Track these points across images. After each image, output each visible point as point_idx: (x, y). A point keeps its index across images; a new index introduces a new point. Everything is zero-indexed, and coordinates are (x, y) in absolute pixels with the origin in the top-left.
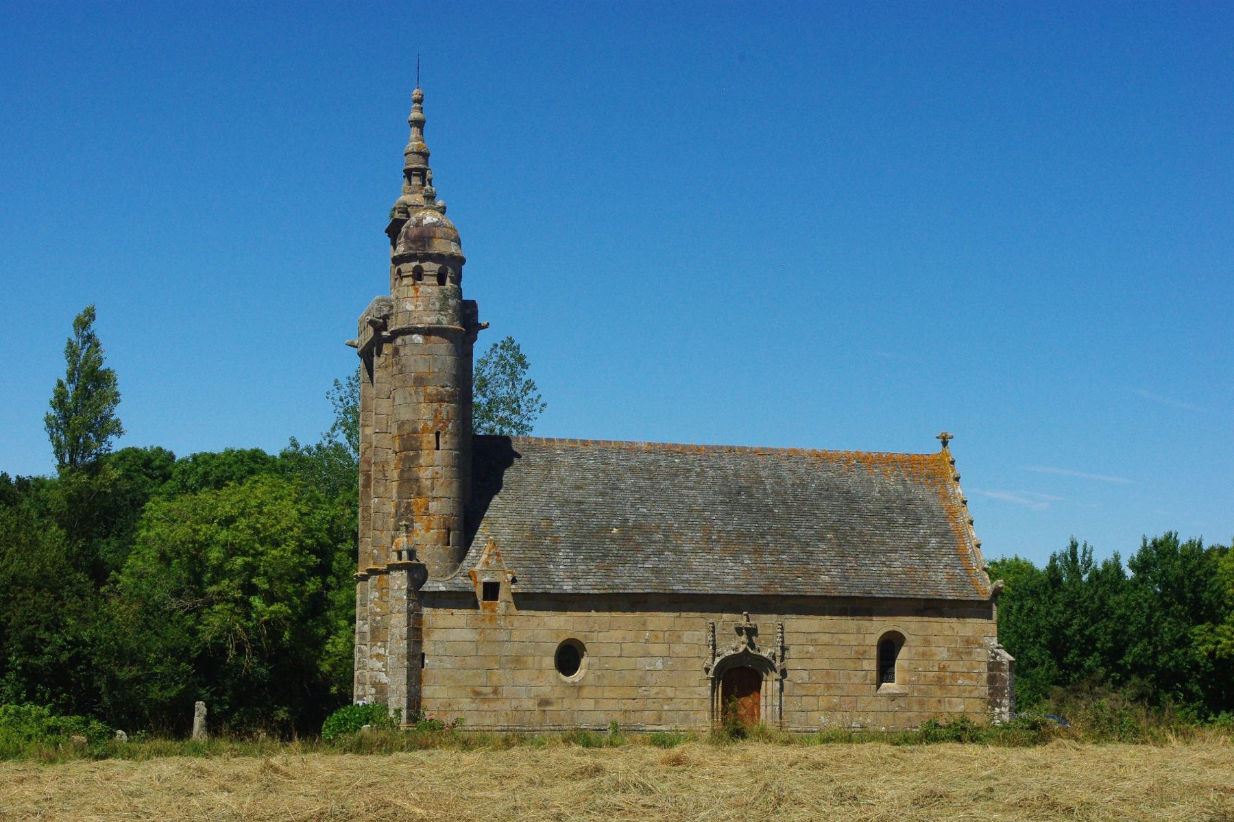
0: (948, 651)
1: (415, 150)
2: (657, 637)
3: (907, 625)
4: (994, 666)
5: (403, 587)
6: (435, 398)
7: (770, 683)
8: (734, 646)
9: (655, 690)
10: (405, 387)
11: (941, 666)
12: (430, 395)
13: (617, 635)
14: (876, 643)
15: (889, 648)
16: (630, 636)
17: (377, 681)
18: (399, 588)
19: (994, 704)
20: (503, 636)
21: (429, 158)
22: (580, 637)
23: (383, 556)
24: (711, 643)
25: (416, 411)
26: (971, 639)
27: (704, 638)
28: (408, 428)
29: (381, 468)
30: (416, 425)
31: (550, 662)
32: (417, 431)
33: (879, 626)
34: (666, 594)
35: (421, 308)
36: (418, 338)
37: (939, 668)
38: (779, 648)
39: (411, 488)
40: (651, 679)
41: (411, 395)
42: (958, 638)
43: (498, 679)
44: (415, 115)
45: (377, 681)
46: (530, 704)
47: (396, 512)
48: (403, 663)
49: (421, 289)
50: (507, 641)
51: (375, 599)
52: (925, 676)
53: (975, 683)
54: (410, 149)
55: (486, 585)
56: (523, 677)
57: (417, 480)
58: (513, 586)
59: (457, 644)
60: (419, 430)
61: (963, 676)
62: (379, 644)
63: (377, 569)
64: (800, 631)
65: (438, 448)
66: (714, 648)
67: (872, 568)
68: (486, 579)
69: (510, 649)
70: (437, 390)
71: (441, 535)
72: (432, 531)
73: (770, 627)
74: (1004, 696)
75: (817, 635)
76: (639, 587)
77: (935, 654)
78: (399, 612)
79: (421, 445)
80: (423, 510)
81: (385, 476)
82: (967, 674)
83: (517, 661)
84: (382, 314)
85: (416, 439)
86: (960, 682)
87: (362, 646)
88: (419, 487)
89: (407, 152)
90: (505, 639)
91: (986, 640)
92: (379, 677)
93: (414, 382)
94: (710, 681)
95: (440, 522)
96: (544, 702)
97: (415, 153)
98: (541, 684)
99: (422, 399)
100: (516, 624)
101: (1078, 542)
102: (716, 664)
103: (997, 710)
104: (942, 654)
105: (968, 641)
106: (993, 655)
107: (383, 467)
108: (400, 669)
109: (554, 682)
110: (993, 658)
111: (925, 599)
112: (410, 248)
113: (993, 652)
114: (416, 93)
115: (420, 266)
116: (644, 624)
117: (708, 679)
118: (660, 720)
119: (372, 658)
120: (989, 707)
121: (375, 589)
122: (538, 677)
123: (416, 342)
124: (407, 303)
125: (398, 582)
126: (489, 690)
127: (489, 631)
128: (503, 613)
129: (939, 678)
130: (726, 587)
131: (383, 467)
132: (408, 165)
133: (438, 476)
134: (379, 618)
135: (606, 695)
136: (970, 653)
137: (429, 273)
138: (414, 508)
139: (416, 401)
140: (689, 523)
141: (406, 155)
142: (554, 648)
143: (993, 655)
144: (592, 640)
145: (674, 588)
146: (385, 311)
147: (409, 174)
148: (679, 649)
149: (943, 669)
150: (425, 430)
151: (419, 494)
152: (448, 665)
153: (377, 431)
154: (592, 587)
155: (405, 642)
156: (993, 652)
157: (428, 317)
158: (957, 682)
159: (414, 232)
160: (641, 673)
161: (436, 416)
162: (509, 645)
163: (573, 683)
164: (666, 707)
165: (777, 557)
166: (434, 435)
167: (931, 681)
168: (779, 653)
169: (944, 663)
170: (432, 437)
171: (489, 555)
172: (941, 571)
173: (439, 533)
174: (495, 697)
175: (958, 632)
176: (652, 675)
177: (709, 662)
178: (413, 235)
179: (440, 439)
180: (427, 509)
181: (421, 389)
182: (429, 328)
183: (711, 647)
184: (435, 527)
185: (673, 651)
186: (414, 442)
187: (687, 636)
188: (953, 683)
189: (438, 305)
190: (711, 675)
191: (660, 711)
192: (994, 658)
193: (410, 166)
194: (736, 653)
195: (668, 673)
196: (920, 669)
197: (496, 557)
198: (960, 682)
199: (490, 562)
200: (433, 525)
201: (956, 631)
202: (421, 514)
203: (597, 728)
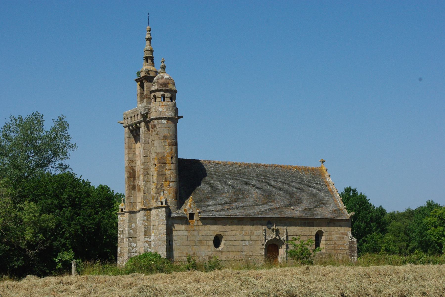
0: (337, 237)
1: (150, 50)
2: (246, 233)
3: (324, 229)
5: (164, 215)
6: (171, 144)
7: (282, 249)
8: (271, 236)
9: (246, 253)
10: (159, 140)
11: (335, 243)
12: (169, 143)
13: (234, 232)
14: (315, 235)
15: (319, 236)
16: (238, 233)
17: (147, 251)
18: (162, 215)
19: (351, 255)
20: (196, 233)
21: (153, 52)
22: (221, 233)
23: (147, 204)
24: (264, 235)
25: (164, 149)
26: (344, 233)
27: (262, 233)
28: (161, 155)
29: (146, 170)
30: (164, 154)
31: (212, 243)
32: (165, 156)
33: (315, 230)
34: (250, 217)
36: (164, 121)
37: (334, 243)
38: (285, 237)
40: (245, 249)
42: (340, 232)
43: (195, 250)
44: (148, 36)
45: (147, 251)
47: (156, 187)
48: (165, 244)
50: (198, 235)
51: (145, 220)
52: (330, 246)
53: (345, 248)
54: (147, 49)
55: (190, 214)
56: (203, 248)
57: (165, 175)
58: (199, 215)
59: (181, 236)
60: (166, 156)
61: (341, 246)
63: (146, 208)
64: (291, 230)
65: (172, 163)
66: (266, 237)
67: (310, 208)
68: (190, 212)
69: (199, 238)
70: (171, 141)
71: (174, 196)
72: (171, 194)
73: (282, 229)
74: (355, 253)
75: (297, 232)
76: (241, 215)
77: (333, 238)
78: (162, 224)
79: (166, 162)
81: (148, 173)
82: (343, 245)
83: (201, 242)
84: (146, 112)
85: (164, 159)
86: (340, 248)
87: (130, 238)
88: (166, 177)
89: (145, 50)
90: (197, 234)
91: (348, 233)
93: (163, 138)
94: (264, 249)
95: (174, 191)
97: (149, 50)
98: (209, 251)
99: (166, 144)
100: (200, 229)
101: (430, 200)
102: (266, 243)
104: (335, 238)
105: (343, 234)
106: (351, 238)
107: (147, 170)
108: (163, 246)
109: (213, 250)
110: (351, 239)
111: (330, 219)
112: (160, 87)
113: (350, 237)
114: (148, 28)
116: (242, 228)
117: (263, 248)
119: (144, 242)
120: (350, 257)
121: (145, 216)
122: (208, 249)
123: (163, 123)
124: (159, 108)
125: (161, 213)
126: (192, 253)
127: (191, 231)
128: (196, 225)
129: (334, 247)
130: (268, 215)
131: (147, 170)
132: (146, 55)
133: (173, 173)
134: (147, 227)
135: (230, 255)
136: (343, 238)
137: (168, 97)
139: (164, 145)
140: (249, 191)
141: (144, 51)
142: (213, 237)
143: (351, 238)
144: (225, 234)
145: (252, 215)
146: (147, 111)
147: (146, 58)
148: (253, 237)
149: (335, 244)
151: (166, 180)
152: (178, 244)
153: (145, 156)
154: (225, 215)
155: (165, 236)
156: (350, 237)
158: (339, 248)
159: (161, 81)
160: (241, 246)
161: (171, 151)
162: (198, 237)
163: (219, 250)
165: (280, 204)
166: (171, 158)
167: (332, 248)
168: (285, 239)
169: (336, 242)
170: (170, 158)
171: (191, 203)
172: (331, 209)
173: (174, 195)
174: (194, 256)
175: (340, 231)
176: (245, 247)
177: (264, 242)
178: (161, 82)
179: (173, 159)
180: (169, 186)
181: (166, 140)
182: (169, 118)
183: (264, 237)
185: (252, 238)
186: (163, 160)
187: (256, 233)
188: (339, 249)
189: (171, 109)
190: (264, 247)
192: (351, 240)
193: (147, 56)
194: (272, 239)
195: (250, 246)
196: (329, 244)
197: (193, 204)
198: (340, 248)
199: (191, 206)
200: (171, 192)
201: (339, 230)
202: (167, 187)
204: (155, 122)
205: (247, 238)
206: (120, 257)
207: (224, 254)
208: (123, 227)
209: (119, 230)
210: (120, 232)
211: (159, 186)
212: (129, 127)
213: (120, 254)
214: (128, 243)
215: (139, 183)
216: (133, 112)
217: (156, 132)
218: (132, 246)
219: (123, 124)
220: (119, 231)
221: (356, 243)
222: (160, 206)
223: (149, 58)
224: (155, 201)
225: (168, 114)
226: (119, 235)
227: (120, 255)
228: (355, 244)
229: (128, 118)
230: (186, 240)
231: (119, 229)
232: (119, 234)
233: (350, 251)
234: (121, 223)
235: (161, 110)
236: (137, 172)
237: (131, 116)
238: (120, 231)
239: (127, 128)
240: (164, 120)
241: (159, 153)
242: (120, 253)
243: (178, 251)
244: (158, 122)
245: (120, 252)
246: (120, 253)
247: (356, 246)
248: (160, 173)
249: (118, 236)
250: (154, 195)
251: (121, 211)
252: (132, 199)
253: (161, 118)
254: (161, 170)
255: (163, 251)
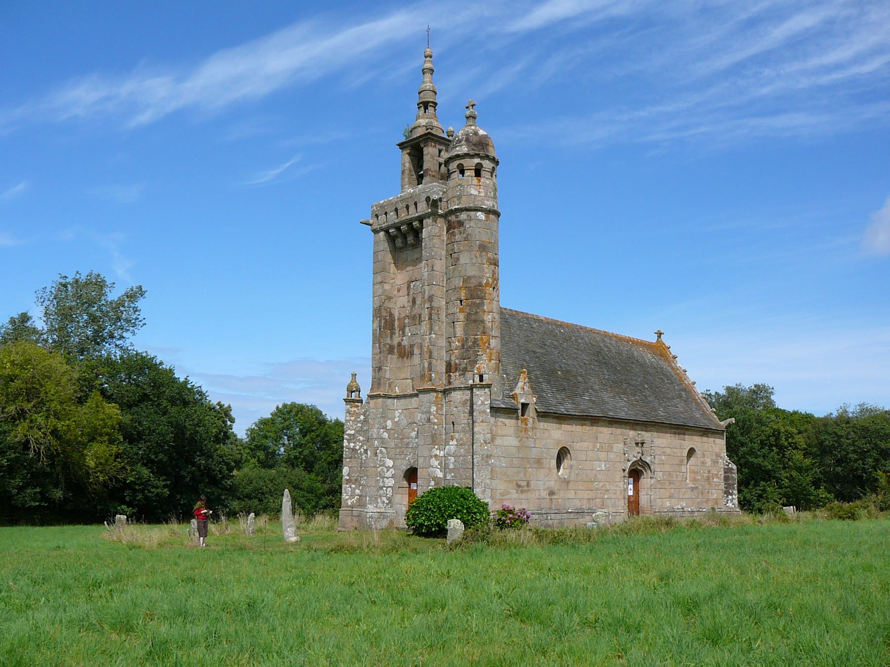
4: (727, 471)
5: (486, 403)
18: (483, 403)
19: (727, 493)
25: (481, 270)
35: (483, 194)
36: (481, 215)
39: (477, 327)
41: (476, 257)
46: (544, 494)
47: (463, 345)
49: (482, 180)
57: (483, 321)
62: (436, 447)
68: (523, 401)
72: (492, 361)
74: (734, 488)
80: (487, 345)
88: (484, 327)
92: (436, 472)
96: (552, 493)
99: (485, 261)
103: (730, 497)
107: (438, 311)
110: (727, 465)
112: (473, 150)
113: (727, 462)
115: (481, 164)
118: (603, 505)
132: (424, 99)
134: (436, 427)
137: (487, 170)
138: (480, 342)
139: (480, 262)
148: (612, 456)
150: (487, 284)
151: (484, 333)
156: (727, 462)
157: (488, 201)
164: (606, 497)
178: (474, 140)
181: (483, 254)
184: (494, 359)
186: (479, 293)
191: (603, 499)
203: (577, 511)
204: (462, 215)
205: (602, 455)
206: (348, 486)
207: (571, 485)
208: (355, 427)
209: (347, 433)
210: (348, 437)
211: (470, 344)
212: (387, 231)
213: (347, 480)
214: (379, 459)
215: (402, 340)
216: (401, 201)
217: (465, 236)
218: (387, 466)
219: (371, 225)
220: (347, 435)
221: (736, 471)
222: (479, 384)
223: (431, 104)
224: (460, 375)
225: (488, 203)
226: (345, 443)
227: (348, 481)
228: (735, 473)
229: (386, 214)
230: (517, 456)
231: (347, 431)
232: (347, 440)
233: (726, 486)
234: (351, 420)
235: (477, 193)
236: (399, 319)
237: (396, 209)
238: (349, 435)
239: (382, 234)
240: (480, 213)
241: (469, 278)
242: (348, 478)
243: (504, 477)
244: (468, 216)
245: (348, 475)
246: (348, 478)
247: (735, 476)
248: (473, 317)
249: (344, 445)
250: (457, 361)
251: (480, 381)
252: (388, 372)
253: (476, 210)
254: (475, 311)
255: (484, 476)
